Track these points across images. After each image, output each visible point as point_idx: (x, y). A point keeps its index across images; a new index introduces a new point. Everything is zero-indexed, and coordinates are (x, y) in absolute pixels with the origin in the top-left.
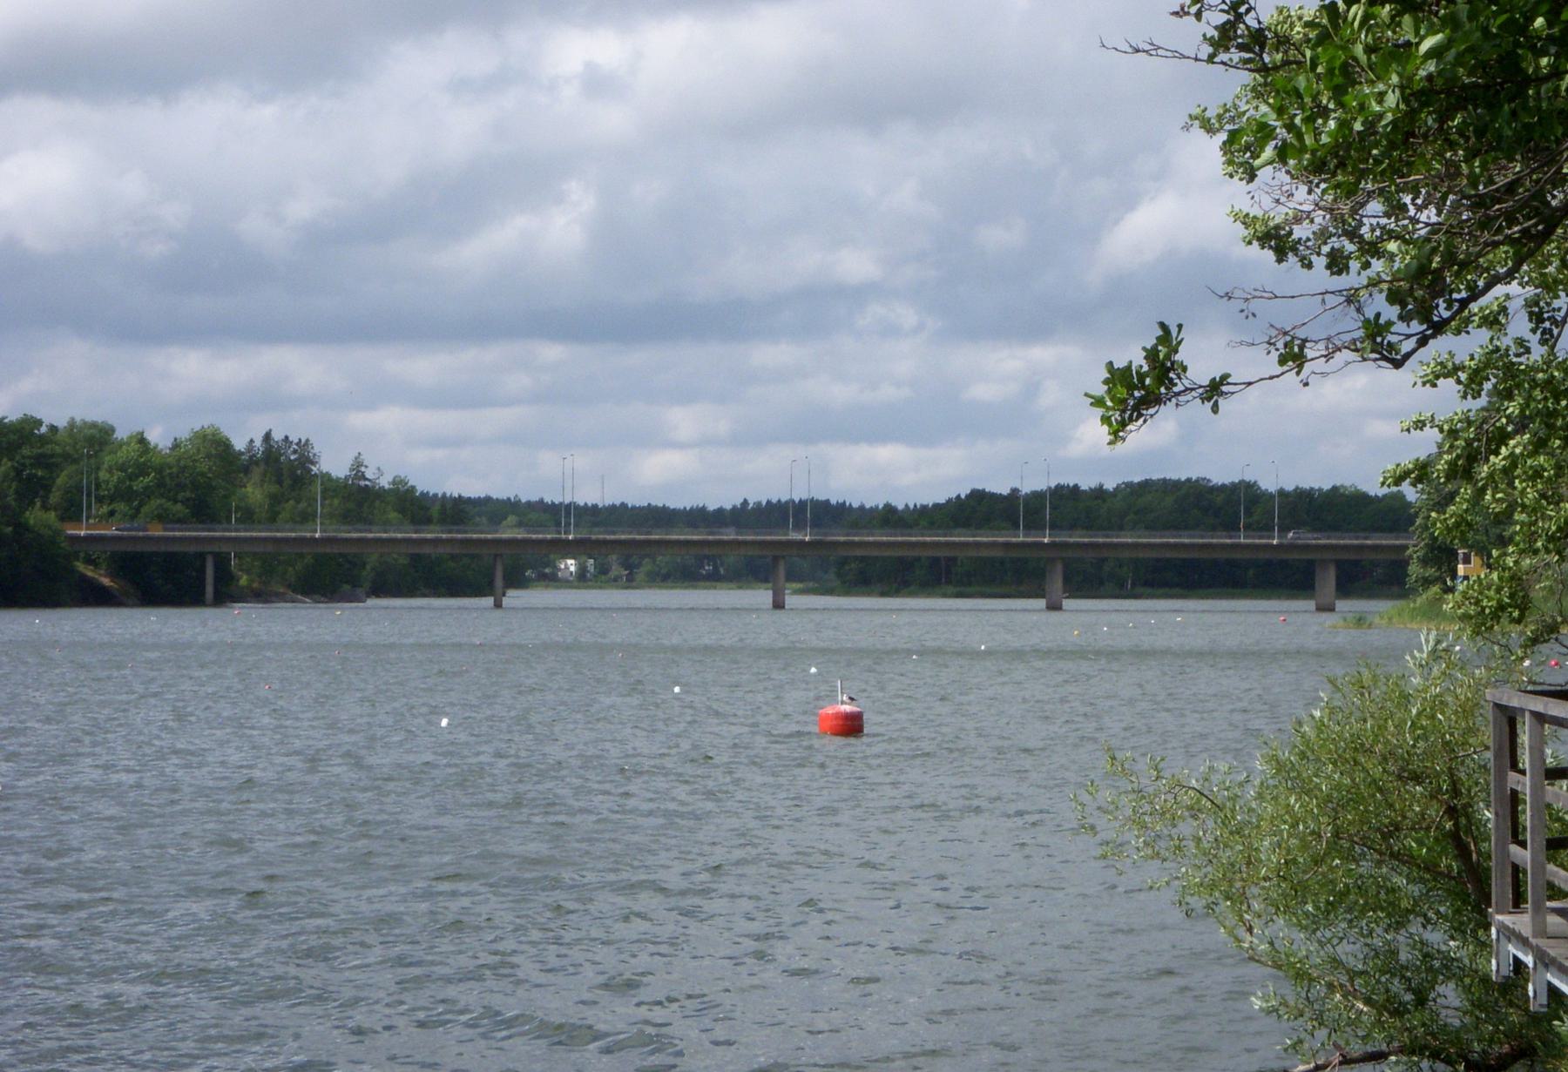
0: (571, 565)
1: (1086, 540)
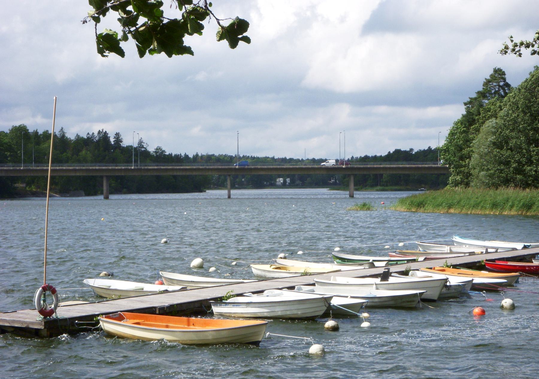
0: (281, 180)
1: (362, 166)
